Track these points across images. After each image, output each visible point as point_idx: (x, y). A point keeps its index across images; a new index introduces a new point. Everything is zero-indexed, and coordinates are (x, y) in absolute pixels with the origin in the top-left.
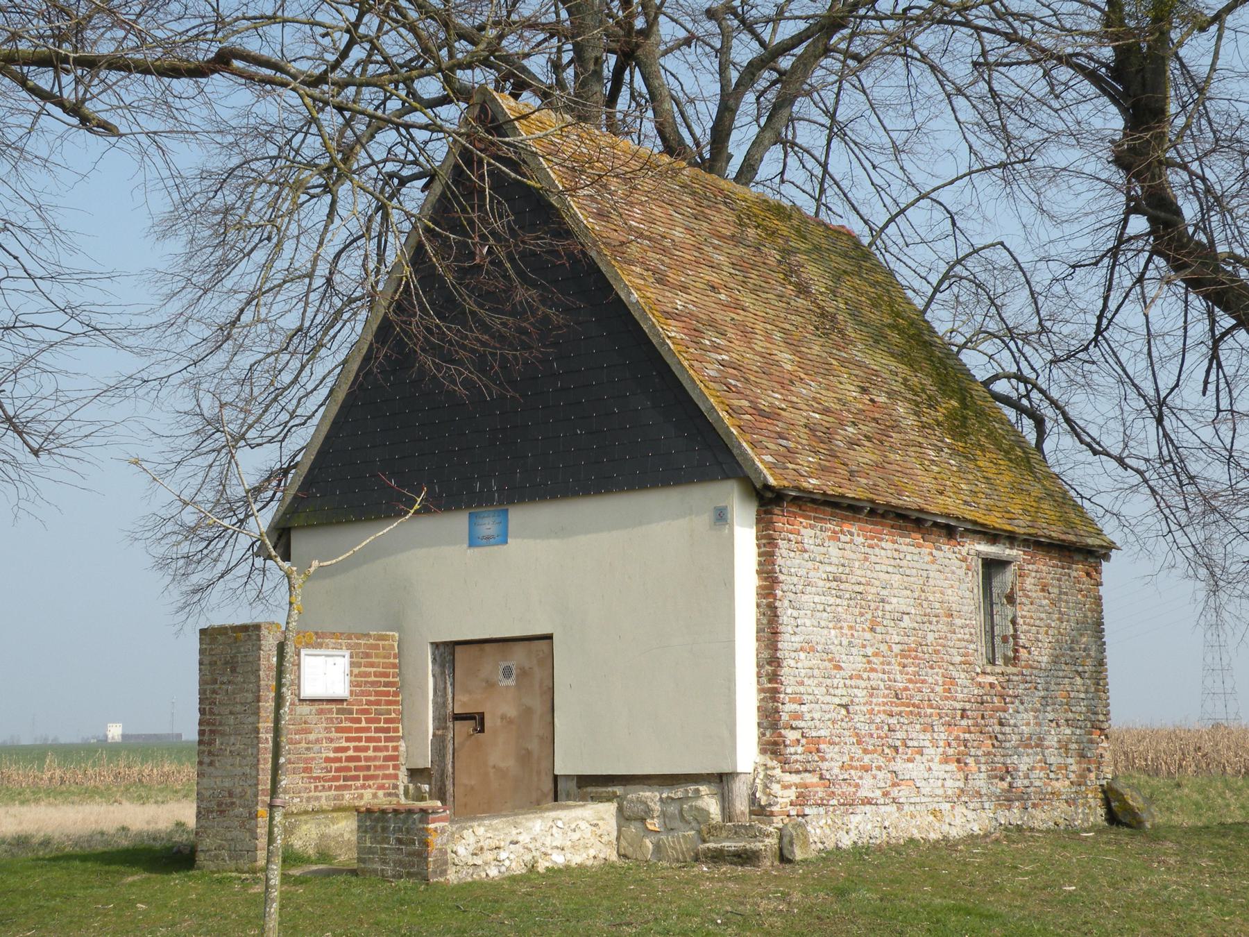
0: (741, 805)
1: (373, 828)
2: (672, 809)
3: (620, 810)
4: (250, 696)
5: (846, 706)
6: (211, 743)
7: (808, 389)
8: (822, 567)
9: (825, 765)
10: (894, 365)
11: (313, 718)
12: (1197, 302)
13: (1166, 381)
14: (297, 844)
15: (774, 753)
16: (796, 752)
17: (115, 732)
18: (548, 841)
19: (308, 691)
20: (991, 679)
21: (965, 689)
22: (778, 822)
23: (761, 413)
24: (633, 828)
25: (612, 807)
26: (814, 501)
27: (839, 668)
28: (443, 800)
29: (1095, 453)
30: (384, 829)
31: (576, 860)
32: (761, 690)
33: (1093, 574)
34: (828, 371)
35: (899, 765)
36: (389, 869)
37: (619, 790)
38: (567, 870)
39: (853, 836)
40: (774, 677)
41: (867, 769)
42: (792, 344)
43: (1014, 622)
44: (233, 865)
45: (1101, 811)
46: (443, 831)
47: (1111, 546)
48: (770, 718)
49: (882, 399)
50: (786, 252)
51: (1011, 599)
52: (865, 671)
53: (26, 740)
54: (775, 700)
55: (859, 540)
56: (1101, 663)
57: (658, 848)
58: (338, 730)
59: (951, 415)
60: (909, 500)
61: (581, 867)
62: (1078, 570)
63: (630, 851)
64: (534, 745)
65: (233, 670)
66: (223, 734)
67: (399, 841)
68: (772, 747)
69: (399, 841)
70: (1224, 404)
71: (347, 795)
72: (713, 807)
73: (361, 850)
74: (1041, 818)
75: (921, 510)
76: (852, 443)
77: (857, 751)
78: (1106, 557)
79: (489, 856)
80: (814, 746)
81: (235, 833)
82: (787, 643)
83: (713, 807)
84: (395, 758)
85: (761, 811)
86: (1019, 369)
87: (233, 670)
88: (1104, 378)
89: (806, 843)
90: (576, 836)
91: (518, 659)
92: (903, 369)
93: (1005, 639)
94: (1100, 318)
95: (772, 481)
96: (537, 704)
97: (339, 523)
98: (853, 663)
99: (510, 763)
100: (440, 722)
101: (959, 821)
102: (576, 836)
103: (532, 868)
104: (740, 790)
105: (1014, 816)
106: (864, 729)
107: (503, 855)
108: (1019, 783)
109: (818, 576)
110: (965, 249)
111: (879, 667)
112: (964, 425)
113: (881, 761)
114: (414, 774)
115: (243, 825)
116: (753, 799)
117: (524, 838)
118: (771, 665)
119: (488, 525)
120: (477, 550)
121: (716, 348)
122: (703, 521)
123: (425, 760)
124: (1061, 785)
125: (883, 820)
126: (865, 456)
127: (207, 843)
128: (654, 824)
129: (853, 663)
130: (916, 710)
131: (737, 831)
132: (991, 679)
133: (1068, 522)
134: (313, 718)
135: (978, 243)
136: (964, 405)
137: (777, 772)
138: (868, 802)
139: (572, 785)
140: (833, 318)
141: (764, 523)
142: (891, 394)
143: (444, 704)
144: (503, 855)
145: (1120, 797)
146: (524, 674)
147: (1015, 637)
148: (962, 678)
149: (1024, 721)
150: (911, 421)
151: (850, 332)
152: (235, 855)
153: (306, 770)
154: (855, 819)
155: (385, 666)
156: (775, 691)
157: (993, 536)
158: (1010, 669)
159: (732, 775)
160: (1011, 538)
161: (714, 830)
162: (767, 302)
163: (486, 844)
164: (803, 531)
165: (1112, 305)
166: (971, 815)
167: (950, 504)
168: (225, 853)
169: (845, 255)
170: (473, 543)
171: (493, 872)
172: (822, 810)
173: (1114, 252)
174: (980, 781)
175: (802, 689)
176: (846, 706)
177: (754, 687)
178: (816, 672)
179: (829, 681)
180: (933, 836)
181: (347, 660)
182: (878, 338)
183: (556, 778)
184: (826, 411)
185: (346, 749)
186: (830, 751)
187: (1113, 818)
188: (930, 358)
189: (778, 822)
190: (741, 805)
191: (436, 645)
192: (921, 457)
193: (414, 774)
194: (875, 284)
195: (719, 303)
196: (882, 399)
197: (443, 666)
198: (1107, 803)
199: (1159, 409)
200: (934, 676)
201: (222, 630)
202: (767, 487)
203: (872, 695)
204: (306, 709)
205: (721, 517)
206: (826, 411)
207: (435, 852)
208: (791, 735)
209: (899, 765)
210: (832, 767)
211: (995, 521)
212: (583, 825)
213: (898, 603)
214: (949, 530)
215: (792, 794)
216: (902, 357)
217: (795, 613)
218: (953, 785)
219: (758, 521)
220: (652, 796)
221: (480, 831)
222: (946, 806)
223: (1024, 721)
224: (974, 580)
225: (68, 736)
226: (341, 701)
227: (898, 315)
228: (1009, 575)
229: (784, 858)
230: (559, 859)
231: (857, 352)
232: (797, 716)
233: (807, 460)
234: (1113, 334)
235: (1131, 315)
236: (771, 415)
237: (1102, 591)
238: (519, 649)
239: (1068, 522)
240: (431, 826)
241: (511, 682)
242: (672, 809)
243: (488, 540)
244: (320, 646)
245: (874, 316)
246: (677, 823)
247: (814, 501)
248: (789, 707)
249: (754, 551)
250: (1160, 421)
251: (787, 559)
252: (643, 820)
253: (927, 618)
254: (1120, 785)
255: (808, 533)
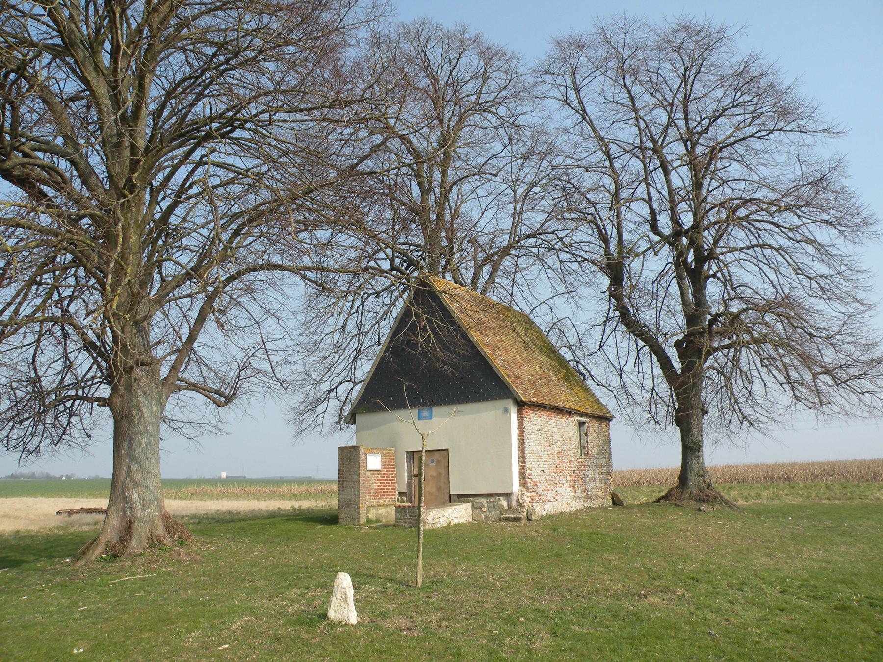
0: (514, 503)
1: (401, 512)
2: (491, 505)
3: (473, 505)
4: (356, 469)
5: (543, 471)
6: (343, 484)
7: (526, 368)
9: (538, 490)
10: (547, 359)
11: (371, 476)
12: (633, 337)
13: (623, 363)
14: (370, 516)
15: (524, 486)
16: (530, 486)
17: (224, 475)
18: (453, 515)
19: (369, 467)
20: (581, 460)
21: (575, 464)
22: (526, 508)
23: (517, 377)
24: (478, 511)
25: (469, 505)
26: (534, 405)
27: (541, 458)
28: (411, 503)
29: (598, 385)
30: (405, 512)
31: (461, 521)
32: (519, 466)
33: (608, 425)
34: (530, 362)
35: (558, 489)
36: (407, 525)
37: (472, 499)
38: (458, 524)
39: (546, 512)
40: (523, 462)
41: (549, 490)
42: (519, 354)
43: (587, 442)
44: (352, 523)
45: (611, 501)
47: (613, 417)
48: (523, 475)
49: (546, 371)
50: (512, 322)
51: (586, 434)
53: (195, 477)
54: (524, 469)
55: (546, 417)
56: (610, 454)
57: (486, 517)
58: (378, 480)
59: (565, 375)
60: (560, 404)
61: (462, 523)
62: (604, 424)
63: (476, 518)
64: (442, 485)
65: (350, 461)
66: (347, 481)
67: (410, 516)
68: (523, 484)
69: (410, 516)
70: (640, 371)
71: (381, 501)
72: (504, 503)
73: (397, 518)
74: (595, 504)
75: (563, 407)
76: (541, 386)
77: (546, 485)
78: (611, 420)
79: (437, 520)
80: (535, 484)
81: (353, 513)
82: (527, 451)
83: (504, 503)
84: (394, 489)
85: (520, 505)
87: (350, 461)
88: (600, 360)
89: (535, 514)
90: (461, 514)
91: (436, 456)
92: (549, 360)
93: (584, 448)
94: (601, 342)
95: (524, 399)
96: (443, 472)
97: (373, 412)
98: (545, 457)
99: (434, 490)
100: (409, 477)
101: (574, 506)
102: (461, 514)
103: (449, 524)
104: (514, 498)
105: (588, 504)
106: (548, 478)
107: (441, 520)
108: (589, 493)
109: (535, 429)
110: (555, 320)
112: (568, 378)
113: (553, 488)
114: (400, 494)
115: (355, 510)
116: (518, 501)
117: (446, 515)
118: (522, 457)
119: (425, 413)
120: (421, 421)
121: (500, 355)
122: (500, 412)
123: (404, 489)
124: (600, 493)
126: (545, 390)
127: (342, 516)
128: (484, 510)
129: (545, 457)
130: (561, 471)
131: (513, 512)
132: (581, 460)
133: (601, 410)
134: (371, 476)
135: (560, 317)
136: (568, 372)
137: (525, 492)
138: (550, 501)
139: (456, 498)
140: (528, 344)
141: (520, 412)
142: (548, 369)
143: (411, 472)
144: (441, 520)
145: (617, 496)
146: (438, 462)
147: (587, 447)
148: (574, 460)
149: (590, 473)
150: (555, 378)
151: (533, 348)
152: (353, 520)
153: (370, 493)
154: (546, 506)
155: (392, 459)
156: (524, 466)
157: (581, 414)
158: (586, 457)
159: (511, 494)
160: (586, 415)
161: (505, 511)
162: (510, 339)
163: (436, 516)
165: (605, 338)
166: (577, 504)
167: (569, 405)
168: (349, 519)
169: (527, 323)
170: (420, 418)
171: (438, 526)
173: (605, 322)
174: (579, 493)
176: (543, 471)
177: (517, 465)
180: (567, 511)
181: (380, 457)
182: (541, 351)
183: (450, 495)
184: (532, 375)
185: (380, 486)
186: (539, 485)
187: (614, 503)
188: (555, 356)
189: (526, 508)
190: (514, 503)
191: (407, 452)
192: (560, 390)
193: (400, 494)
194: (536, 332)
195: (497, 340)
196: (546, 371)
197: (410, 459)
198: (613, 498)
199: (620, 372)
200: (566, 460)
201: (346, 448)
202: (522, 401)
204: (368, 473)
205: (506, 410)
206: (532, 375)
208: (529, 480)
209: (558, 489)
210: (540, 491)
211: (582, 409)
212: (463, 510)
213: (556, 437)
214: (569, 413)
215: (529, 499)
216: (548, 356)
218: (572, 494)
219: (518, 412)
220: (484, 501)
221: (434, 512)
222: (570, 501)
223: (590, 473)
224: (576, 429)
225: (208, 476)
226: (379, 470)
227: (544, 342)
228: (585, 427)
229: (528, 519)
230: (456, 521)
231: (536, 355)
232: (530, 474)
233: (531, 392)
234: (605, 347)
235: (611, 341)
236: (518, 377)
237: (610, 431)
238: (436, 453)
239: (601, 410)
241: (434, 464)
242: (491, 505)
243: (425, 418)
244: (372, 453)
245: (538, 343)
246: (493, 509)
247: (534, 405)
248: (528, 471)
249: (516, 422)
250: (620, 375)
251: (527, 424)
252: (481, 508)
253: (564, 442)
254: (616, 493)
255: (532, 415)
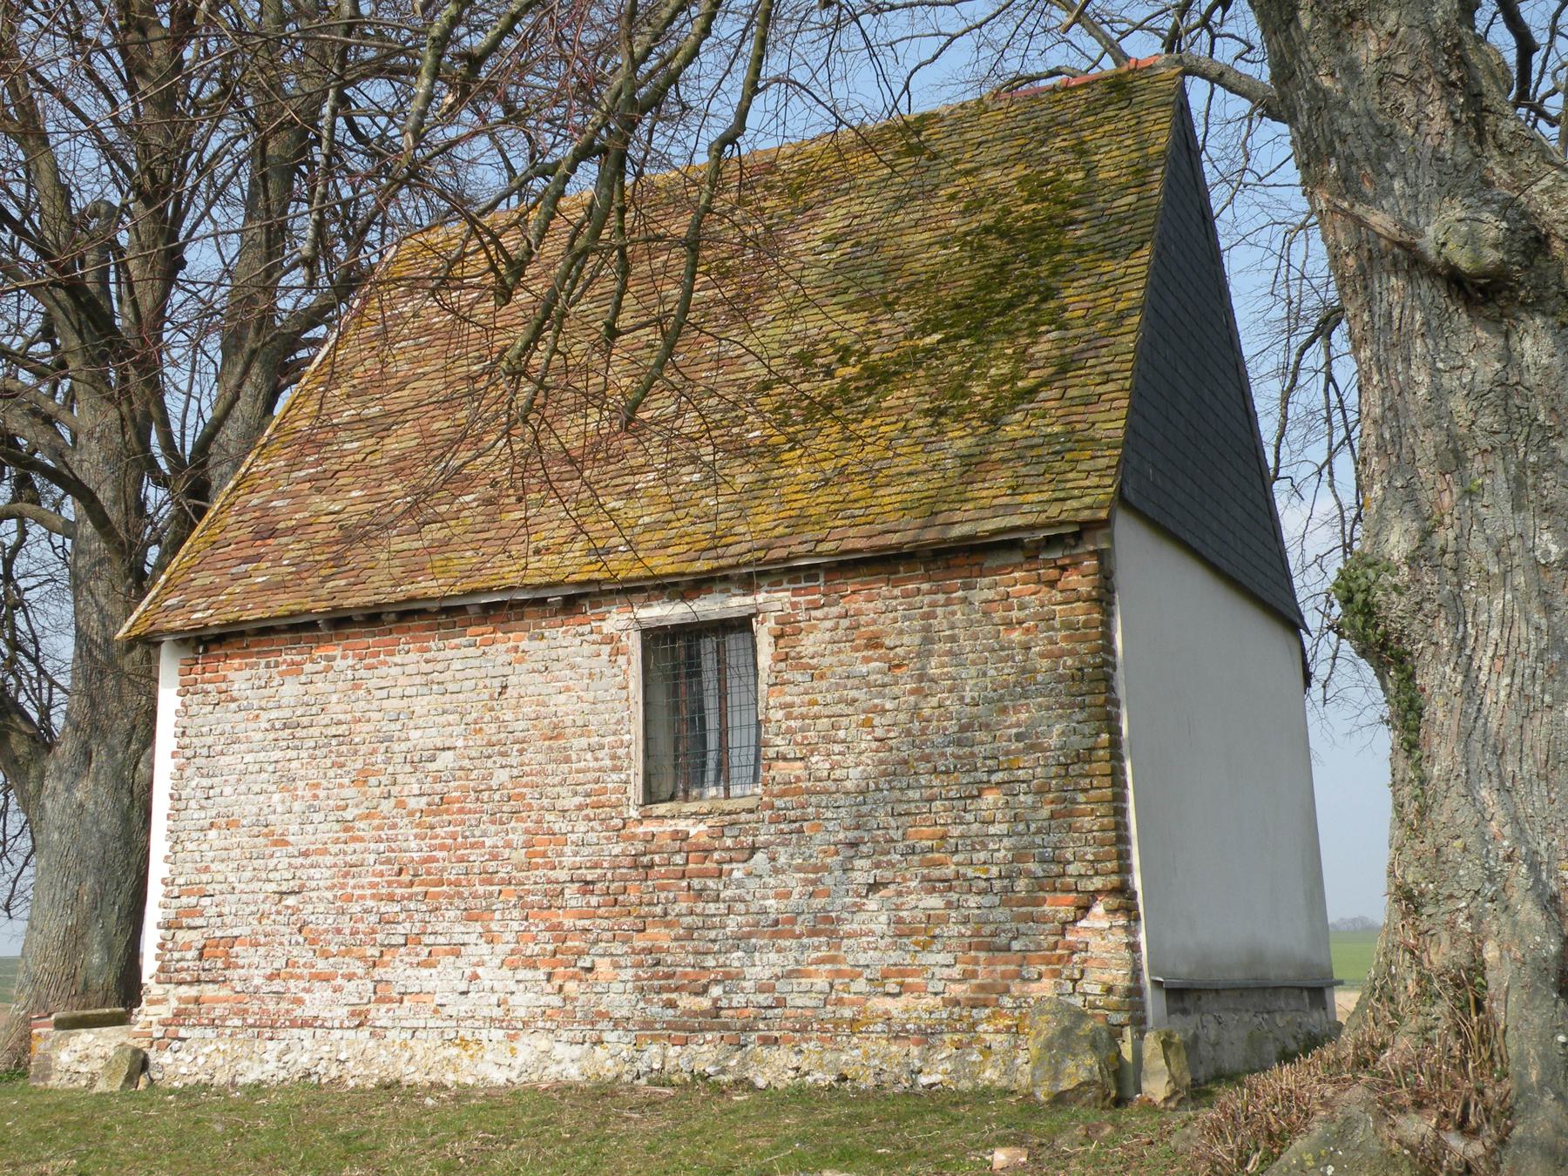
8: (264, 716)
46: (47, 1037)
52: (336, 841)
86: (1311, 341)
111: (367, 835)
125: (338, 1051)
164: (231, 675)
172: (210, 1033)
175: (205, 877)
178: (236, 853)
179: (258, 863)
203: (345, 875)
207: (36, 1057)
217: (206, 782)
240: (35, 1031)
